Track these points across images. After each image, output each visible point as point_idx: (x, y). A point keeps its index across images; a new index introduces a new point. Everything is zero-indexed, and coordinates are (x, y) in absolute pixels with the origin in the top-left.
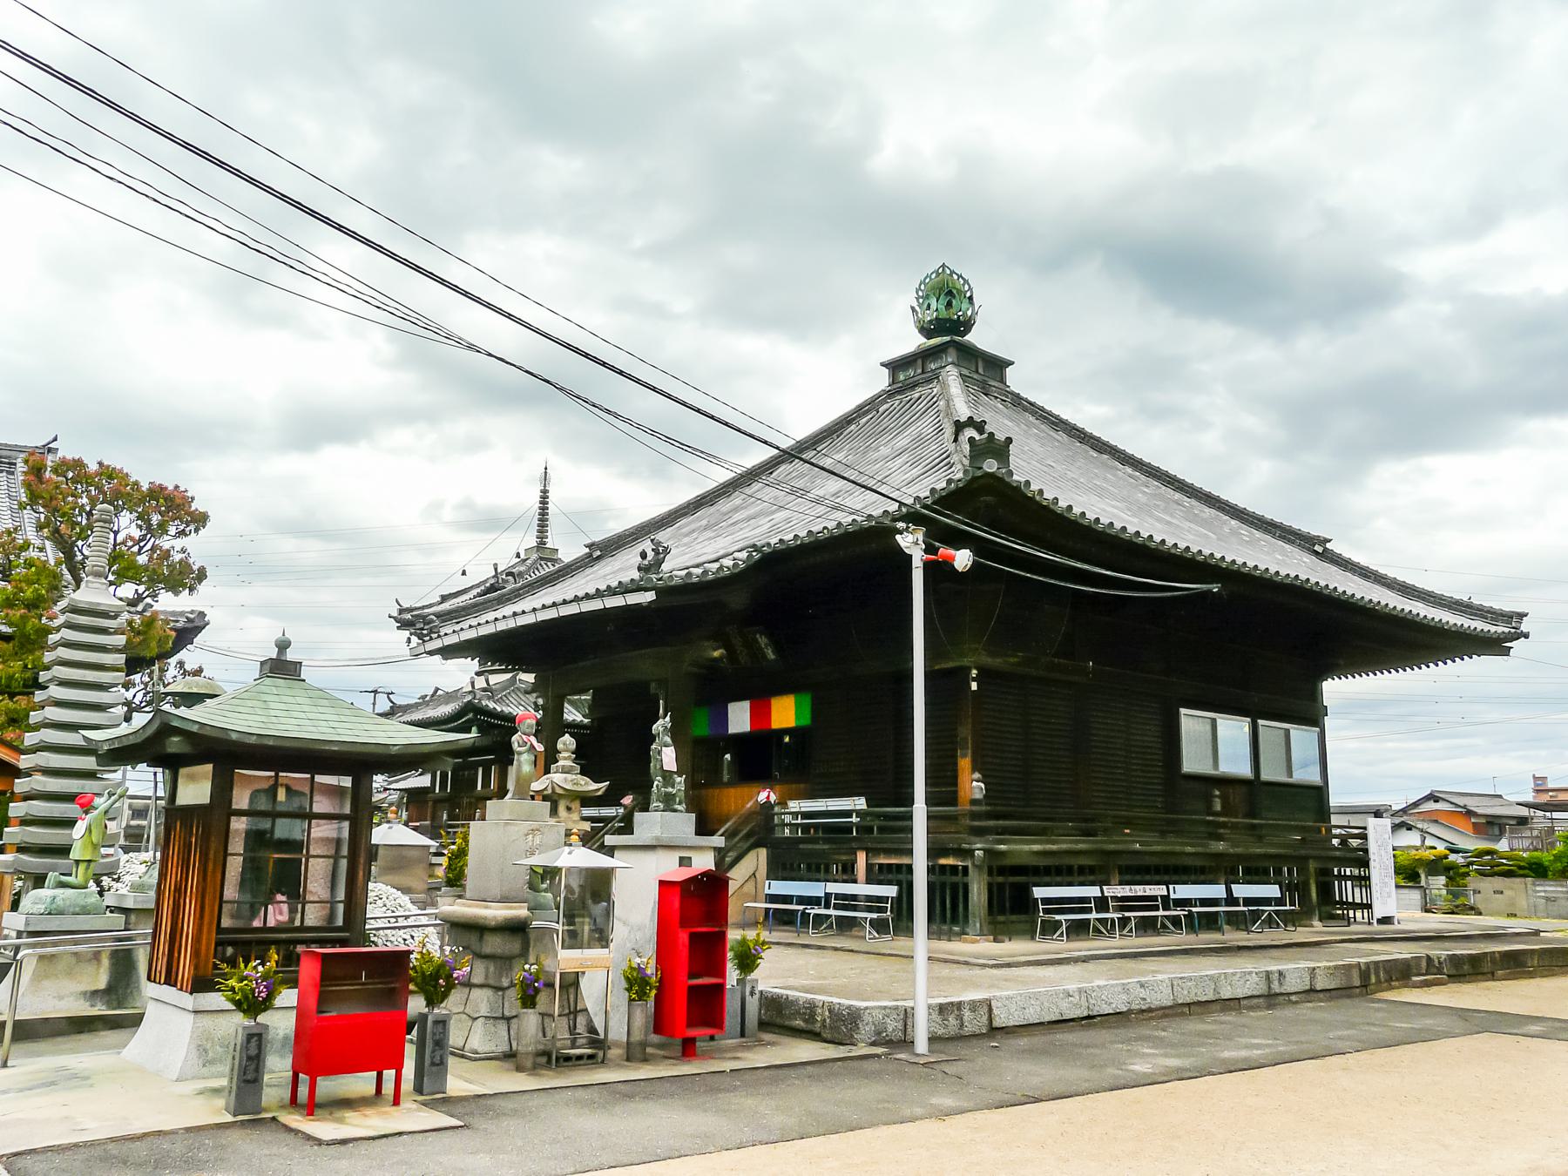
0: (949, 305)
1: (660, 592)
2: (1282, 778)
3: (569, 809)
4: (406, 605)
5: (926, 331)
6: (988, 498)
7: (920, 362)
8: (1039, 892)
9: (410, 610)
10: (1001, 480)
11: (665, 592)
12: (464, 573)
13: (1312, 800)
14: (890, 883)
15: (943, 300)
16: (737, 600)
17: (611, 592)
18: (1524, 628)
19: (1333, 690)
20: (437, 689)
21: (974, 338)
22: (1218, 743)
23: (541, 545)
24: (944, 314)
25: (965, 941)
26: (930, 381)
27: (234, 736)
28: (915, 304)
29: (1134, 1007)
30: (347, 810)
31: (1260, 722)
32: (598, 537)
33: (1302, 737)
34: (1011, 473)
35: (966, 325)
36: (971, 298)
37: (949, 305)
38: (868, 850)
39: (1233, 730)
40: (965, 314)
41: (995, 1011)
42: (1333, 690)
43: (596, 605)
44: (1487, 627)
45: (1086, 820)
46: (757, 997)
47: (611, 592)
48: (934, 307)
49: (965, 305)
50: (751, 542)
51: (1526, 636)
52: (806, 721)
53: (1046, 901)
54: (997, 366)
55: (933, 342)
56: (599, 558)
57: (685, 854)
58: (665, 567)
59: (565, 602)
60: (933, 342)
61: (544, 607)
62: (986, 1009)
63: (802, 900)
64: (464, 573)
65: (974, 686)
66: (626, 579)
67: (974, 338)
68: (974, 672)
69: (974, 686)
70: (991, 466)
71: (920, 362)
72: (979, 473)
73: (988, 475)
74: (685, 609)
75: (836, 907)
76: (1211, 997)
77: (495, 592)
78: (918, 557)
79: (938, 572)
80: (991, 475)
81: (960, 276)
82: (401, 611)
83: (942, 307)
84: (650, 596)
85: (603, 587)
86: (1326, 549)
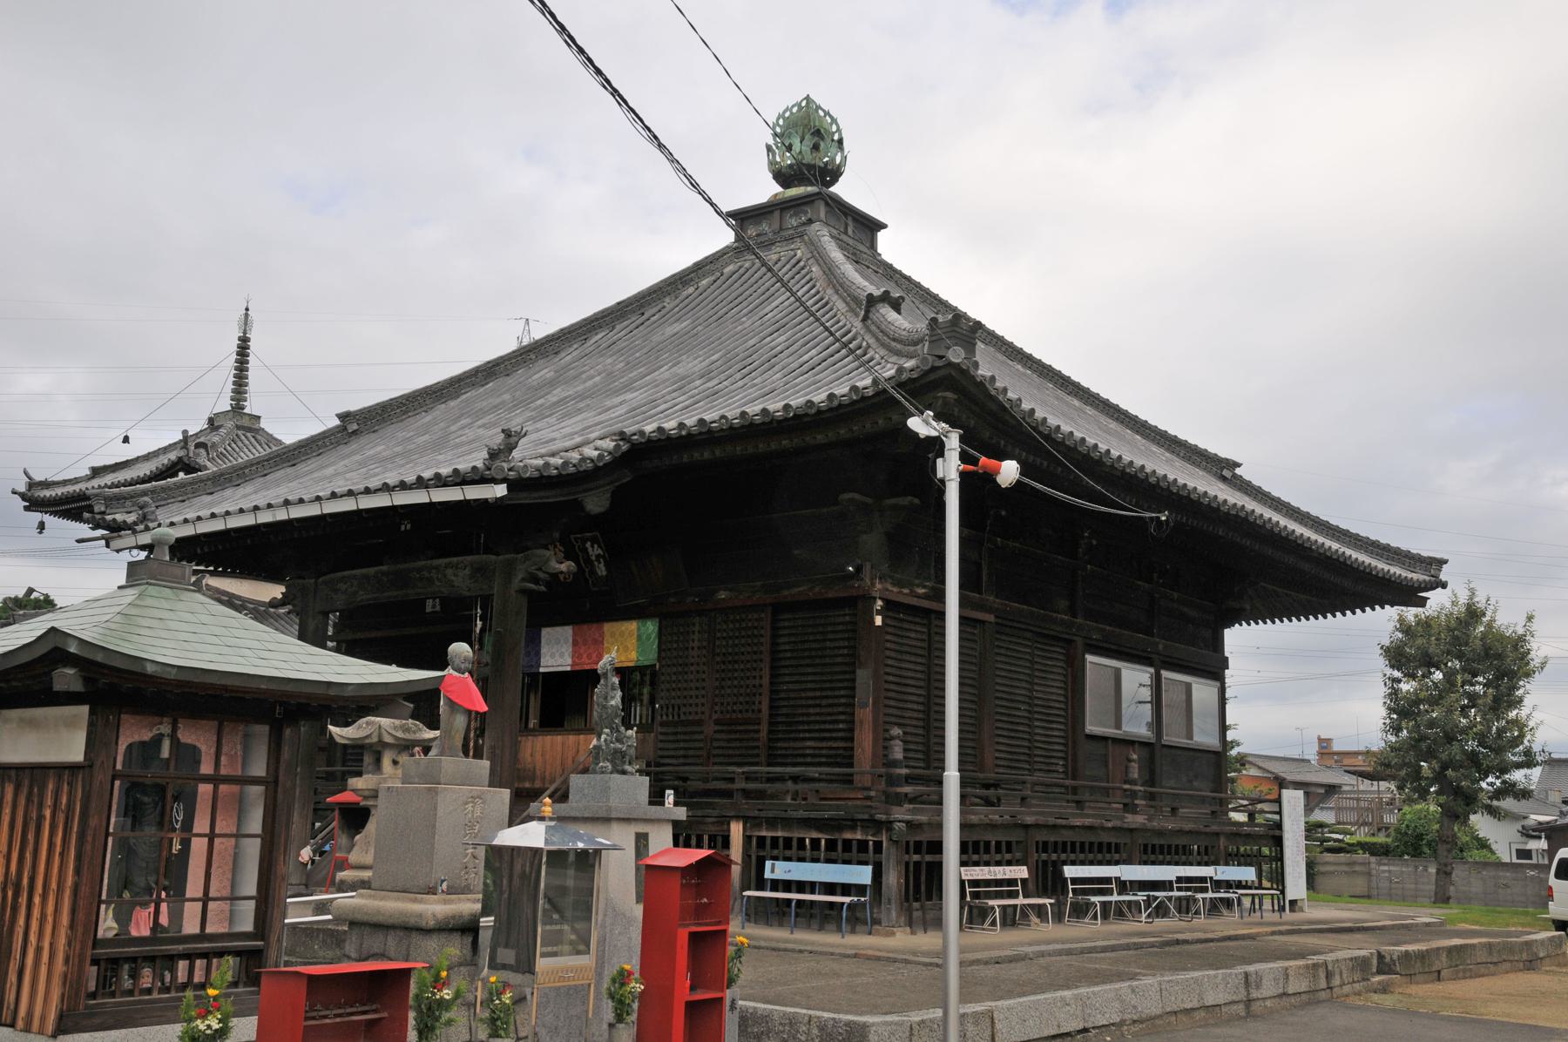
0: (816, 147)
1: (515, 485)
2: (1183, 741)
3: (395, 763)
4: (38, 477)
5: (783, 177)
6: (949, 394)
7: (777, 214)
8: (1070, 871)
9: (46, 484)
10: (964, 373)
11: (515, 485)
12: (126, 440)
13: (1218, 763)
14: (1018, 863)
15: (809, 141)
16: (596, 503)
17: (421, 483)
18: (1443, 577)
19: (1238, 639)
20: (31, 591)
21: (840, 189)
22: (1124, 694)
23: (238, 408)
24: (809, 158)
25: (878, 934)
26: (791, 239)
27: (150, 669)
28: (771, 142)
29: (1127, 1017)
30: (259, 769)
31: (1165, 674)
32: (354, 406)
33: (1203, 691)
34: (976, 365)
35: (834, 174)
36: (840, 141)
37: (816, 147)
38: (746, 819)
39: (1135, 678)
40: (833, 160)
41: (998, 1026)
42: (1238, 639)
43: (419, 497)
44: (1405, 574)
45: (987, 786)
46: (736, 1013)
47: (440, 481)
48: (797, 147)
49: (834, 149)
50: (617, 427)
51: (1444, 585)
52: (650, 657)
53: (1075, 881)
54: (871, 227)
55: (794, 192)
56: (354, 432)
57: (642, 828)
58: (516, 454)
59: (367, 491)
60: (794, 192)
61: (334, 495)
62: (988, 1021)
63: (830, 888)
64: (126, 440)
65: (878, 621)
66: (464, 466)
67: (840, 189)
68: (880, 603)
69: (878, 621)
70: (956, 355)
71: (777, 214)
72: (939, 363)
73: (950, 364)
74: (541, 506)
75: (1179, 889)
76: (1195, 1004)
77: (179, 469)
78: (949, 468)
79: (976, 486)
80: (956, 366)
81: (827, 113)
82: (32, 485)
83: (806, 148)
84: (500, 491)
85: (427, 474)
86: (1235, 476)
